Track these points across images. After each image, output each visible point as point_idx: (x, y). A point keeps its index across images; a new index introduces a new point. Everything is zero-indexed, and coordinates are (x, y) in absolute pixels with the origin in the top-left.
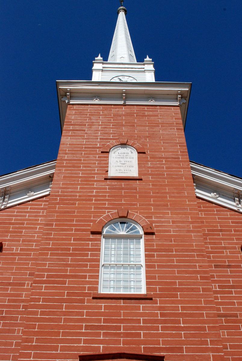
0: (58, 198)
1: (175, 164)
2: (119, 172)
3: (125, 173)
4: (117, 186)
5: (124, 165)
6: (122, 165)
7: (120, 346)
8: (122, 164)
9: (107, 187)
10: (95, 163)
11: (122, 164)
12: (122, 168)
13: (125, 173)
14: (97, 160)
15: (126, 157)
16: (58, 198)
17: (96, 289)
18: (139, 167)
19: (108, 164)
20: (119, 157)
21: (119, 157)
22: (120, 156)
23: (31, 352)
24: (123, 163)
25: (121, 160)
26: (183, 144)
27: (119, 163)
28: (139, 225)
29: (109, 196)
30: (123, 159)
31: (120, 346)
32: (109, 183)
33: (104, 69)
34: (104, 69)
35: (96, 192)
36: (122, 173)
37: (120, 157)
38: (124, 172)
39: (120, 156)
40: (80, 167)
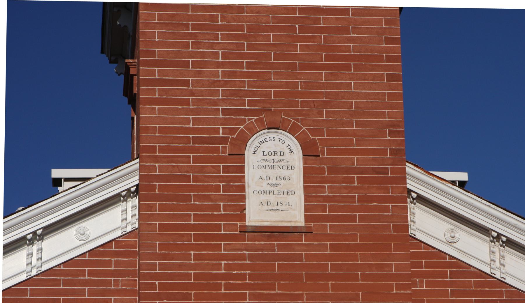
0: (157, 283)
1: (378, 188)
2: (266, 207)
3: (278, 210)
4: (267, 250)
5: (276, 189)
6: (272, 188)
7: (190, 184)
8: (271, 185)
9: (247, 252)
10: (217, 188)
11: (271, 185)
12: (272, 198)
13: (278, 210)
14: (221, 179)
15: (279, 164)
16: (157, 283)
17: (242, 217)
18: (307, 199)
19: (243, 188)
20: (265, 163)
21: (265, 163)
22: (266, 160)
23: (329, 194)
24: (274, 182)
25: (270, 172)
26: (399, 126)
27: (265, 182)
28: (449, 241)
29: (251, 257)
30: (272, 170)
31: (190, 184)
32: (249, 242)
35: (228, 267)
36: (272, 210)
37: (267, 164)
38: (276, 207)
39: (266, 160)
40: (188, 198)
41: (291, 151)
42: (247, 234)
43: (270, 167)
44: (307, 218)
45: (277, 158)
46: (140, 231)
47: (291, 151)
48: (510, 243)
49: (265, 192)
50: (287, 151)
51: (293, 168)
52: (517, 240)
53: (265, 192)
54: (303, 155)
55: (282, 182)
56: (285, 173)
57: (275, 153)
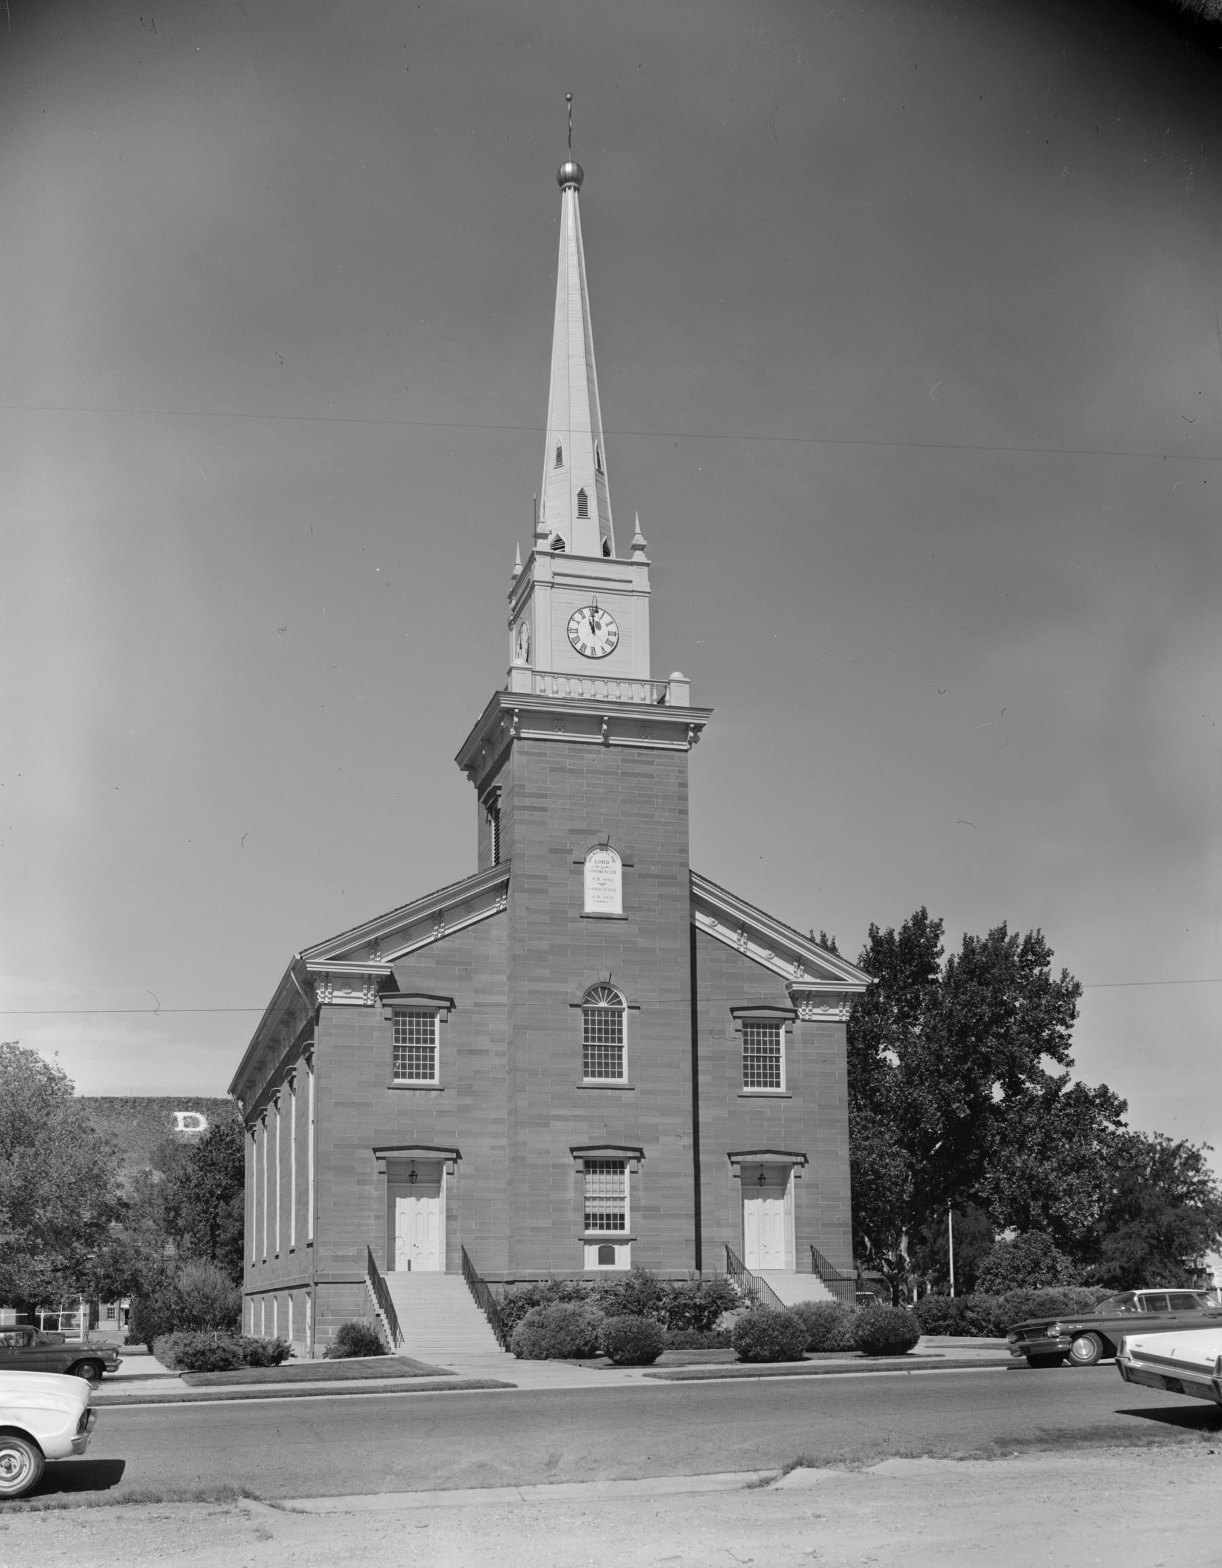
5: (603, 887)
24: (602, 882)
25: (600, 875)
33: (558, 580)
34: (558, 580)
36: (601, 902)
41: (614, 861)
42: (317, 1318)
43: (600, 871)
44: (625, 908)
45: (605, 865)
46: (28, 1316)
47: (614, 861)
48: (528, 589)
49: (596, 889)
50: (611, 861)
51: (615, 872)
52: (1182, 1406)
53: (596, 889)
54: (624, 865)
55: (608, 882)
56: (609, 876)
57: (603, 862)
